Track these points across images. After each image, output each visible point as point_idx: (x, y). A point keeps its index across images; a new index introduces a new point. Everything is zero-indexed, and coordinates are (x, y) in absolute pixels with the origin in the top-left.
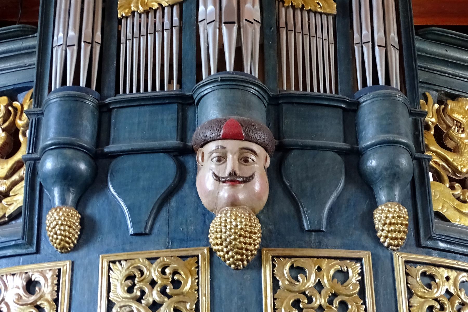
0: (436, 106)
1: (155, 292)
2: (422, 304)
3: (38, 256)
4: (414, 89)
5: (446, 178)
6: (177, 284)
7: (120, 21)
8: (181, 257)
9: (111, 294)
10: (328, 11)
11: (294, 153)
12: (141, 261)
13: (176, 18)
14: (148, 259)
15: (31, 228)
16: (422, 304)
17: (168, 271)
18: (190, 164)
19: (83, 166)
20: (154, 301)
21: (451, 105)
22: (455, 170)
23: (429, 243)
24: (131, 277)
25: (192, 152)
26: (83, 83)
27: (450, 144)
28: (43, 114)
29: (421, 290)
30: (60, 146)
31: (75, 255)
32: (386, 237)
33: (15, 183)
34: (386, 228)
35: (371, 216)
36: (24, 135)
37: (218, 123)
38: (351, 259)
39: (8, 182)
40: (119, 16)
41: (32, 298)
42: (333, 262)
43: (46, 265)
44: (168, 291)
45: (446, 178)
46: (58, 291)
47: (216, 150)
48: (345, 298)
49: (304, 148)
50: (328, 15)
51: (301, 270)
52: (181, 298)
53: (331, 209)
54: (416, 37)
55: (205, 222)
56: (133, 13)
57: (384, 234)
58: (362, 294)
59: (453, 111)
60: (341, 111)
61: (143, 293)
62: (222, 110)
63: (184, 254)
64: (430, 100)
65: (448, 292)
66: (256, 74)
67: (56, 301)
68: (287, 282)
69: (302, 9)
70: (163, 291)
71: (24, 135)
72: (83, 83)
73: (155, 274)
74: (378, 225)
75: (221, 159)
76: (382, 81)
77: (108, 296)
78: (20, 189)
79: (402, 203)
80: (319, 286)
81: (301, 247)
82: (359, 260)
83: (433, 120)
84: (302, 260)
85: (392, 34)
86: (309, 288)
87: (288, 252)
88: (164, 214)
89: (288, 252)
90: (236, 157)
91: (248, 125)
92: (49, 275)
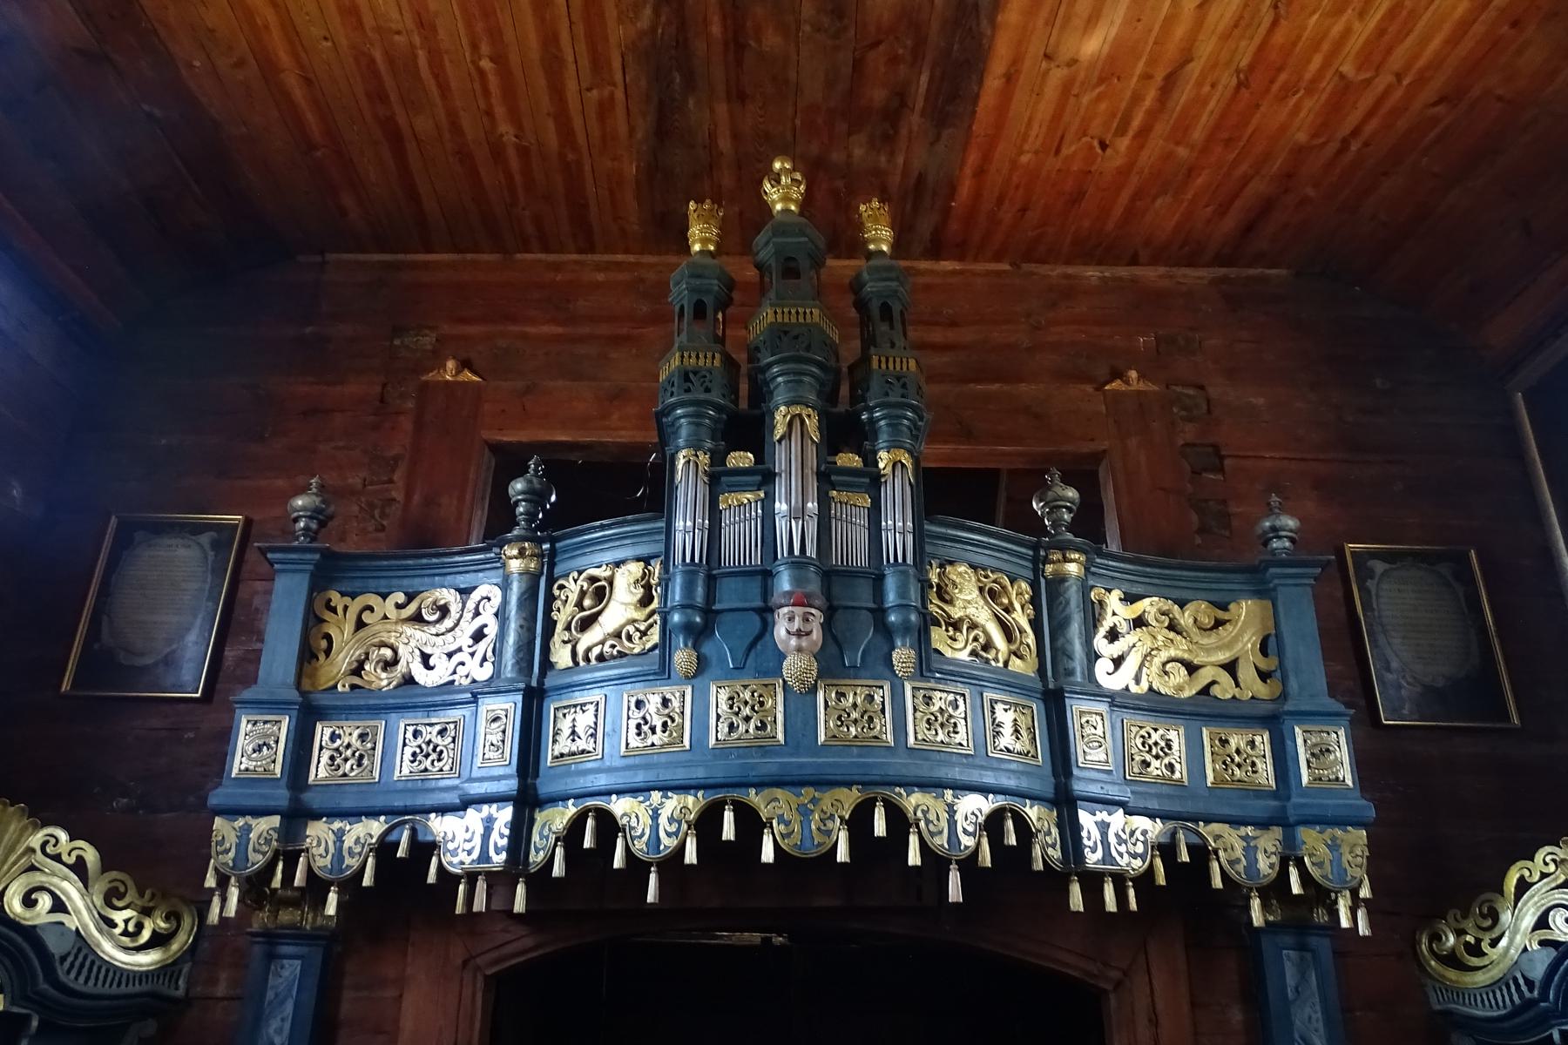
0: (938, 570)
1: (747, 709)
2: (922, 717)
3: (669, 681)
4: (922, 562)
5: (943, 623)
6: (762, 704)
7: (721, 511)
8: (764, 685)
9: (719, 734)
10: (865, 505)
11: (840, 611)
12: (739, 688)
13: (759, 511)
14: (743, 686)
15: (665, 657)
16: (922, 717)
17: (755, 694)
18: (770, 619)
19: (698, 619)
20: (747, 716)
21: (948, 568)
22: (949, 617)
23: (928, 674)
24: (731, 698)
25: (771, 610)
26: (697, 560)
27: (947, 597)
28: (670, 579)
29: (922, 707)
30: (683, 607)
31: (694, 681)
32: (900, 671)
33: (651, 626)
34: (900, 664)
35: (891, 655)
36: (656, 590)
37: (789, 594)
38: (876, 687)
39: (646, 624)
40: (721, 508)
41: (667, 711)
42: (865, 688)
43: (674, 687)
44: (756, 708)
45: (943, 623)
46: (683, 706)
47: (788, 613)
48: (872, 714)
49: (847, 608)
50: (864, 507)
51: (844, 695)
52: (765, 714)
53: (864, 651)
54: (925, 522)
55: (780, 660)
56: (730, 506)
57: (899, 668)
58: (883, 711)
59: (949, 573)
60: (871, 581)
61: (740, 709)
62: (791, 585)
63: (766, 683)
64: (934, 566)
65: (940, 708)
66: (814, 556)
67: (683, 713)
68: (834, 703)
69: (846, 504)
70: (753, 708)
71: (656, 590)
72: (697, 560)
73: (747, 695)
74: (895, 662)
75: (791, 619)
76: (900, 560)
77: (717, 736)
78: (656, 630)
79: (912, 647)
80: (855, 705)
81: (844, 678)
82: (882, 687)
83: (936, 580)
84: (844, 687)
85: (908, 523)
86: (848, 707)
87: (835, 682)
88: (752, 654)
89: (835, 682)
90: (801, 619)
91: (808, 596)
92: (677, 695)
